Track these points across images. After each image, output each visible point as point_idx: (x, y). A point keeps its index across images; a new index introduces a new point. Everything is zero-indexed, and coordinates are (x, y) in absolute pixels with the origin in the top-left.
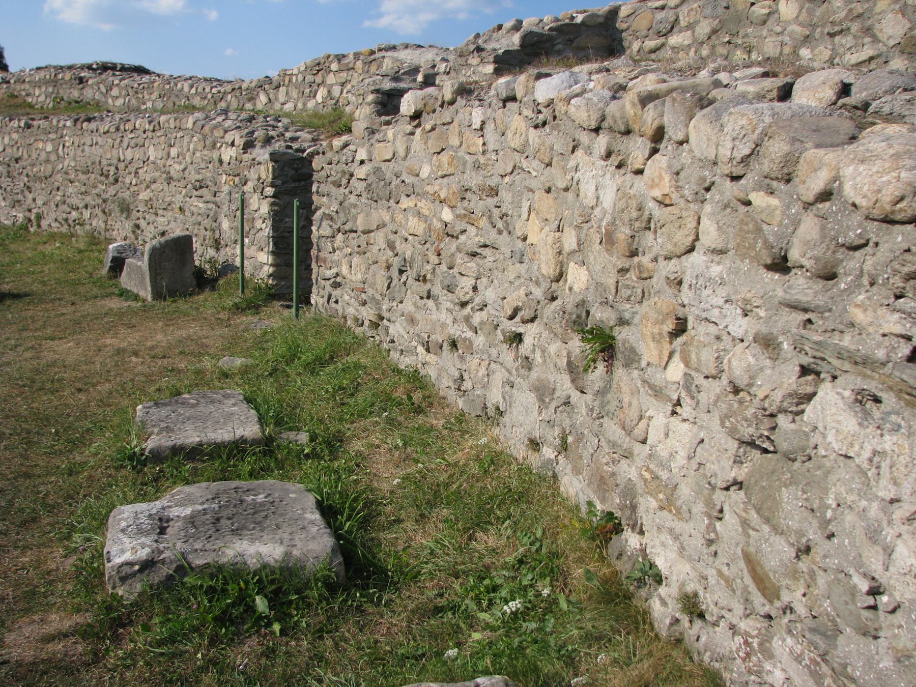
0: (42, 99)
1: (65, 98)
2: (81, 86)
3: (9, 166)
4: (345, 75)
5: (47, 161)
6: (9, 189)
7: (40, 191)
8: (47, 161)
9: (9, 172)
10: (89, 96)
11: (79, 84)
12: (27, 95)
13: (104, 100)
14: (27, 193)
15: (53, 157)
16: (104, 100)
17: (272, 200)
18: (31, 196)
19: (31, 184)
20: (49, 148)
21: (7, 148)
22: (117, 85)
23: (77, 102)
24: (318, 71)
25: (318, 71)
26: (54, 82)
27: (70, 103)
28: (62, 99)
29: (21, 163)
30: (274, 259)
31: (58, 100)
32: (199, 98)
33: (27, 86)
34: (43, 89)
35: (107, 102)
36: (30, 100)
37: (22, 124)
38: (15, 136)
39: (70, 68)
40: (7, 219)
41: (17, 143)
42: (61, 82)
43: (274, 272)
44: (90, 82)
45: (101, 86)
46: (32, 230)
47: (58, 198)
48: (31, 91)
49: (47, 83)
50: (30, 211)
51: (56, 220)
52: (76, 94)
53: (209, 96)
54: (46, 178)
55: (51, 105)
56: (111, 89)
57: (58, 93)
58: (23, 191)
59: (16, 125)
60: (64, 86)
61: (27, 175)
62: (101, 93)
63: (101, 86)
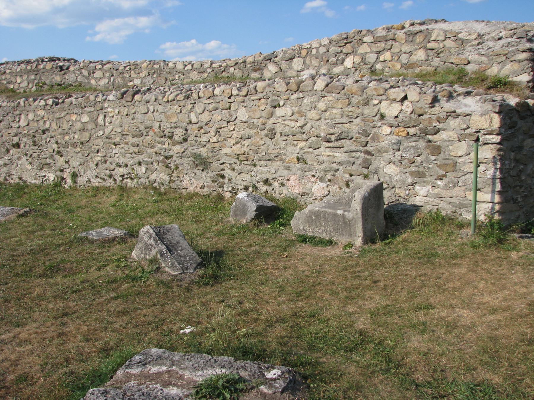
0: (25, 84)
1: (48, 82)
2: (63, 72)
3: (34, 136)
4: (383, 45)
5: (83, 130)
6: (35, 155)
7: (75, 155)
8: (83, 130)
9: (34, 142)
10: (71, 79)
11: (60, 71)
12: (9, 83)
13: (86, 81)
14: (57, 157)
15: (90, 126)
16: (86, 81)
17: (499, 146)
18: (62, 159)
19: (62, 149)
20: (85, 118)
21: (31, 123)
22: (100, 69)
23: (58, 85)
24: (346, 43)
25: (346, 43)
26: (37, 71)
27: (52, 86)
28: (45, 84)
29: (48, 134)
30: (501, 198)
31: (41, 86)
32: (196, 73)
33: (8, 76)
34: (25, 77)
35: (89, 83)
36: (12, 87)
37: (50, 102)
38: (41, 113)
39: (52, 60)
40: (35, 179)
41: (43, 118)
42: (42, 71)
43: (501, 208)
44: (71, 69)
45: (83, 71)
46: (67, 186)
47: (99, 158)
48: (13, 80)
49: (28, 72)
50: (62, 171)
51: (97, 176)
52: (58, 79)
53: (209, 70)
54: (82, 143)
55: (34, 89)
56: (94, 73)
57: (40, 79)
58: (52, 156)
59: (43, 103)
60: (46, 74)
61: (57, 143)
62: (84, 76)
63: (83, 71)
